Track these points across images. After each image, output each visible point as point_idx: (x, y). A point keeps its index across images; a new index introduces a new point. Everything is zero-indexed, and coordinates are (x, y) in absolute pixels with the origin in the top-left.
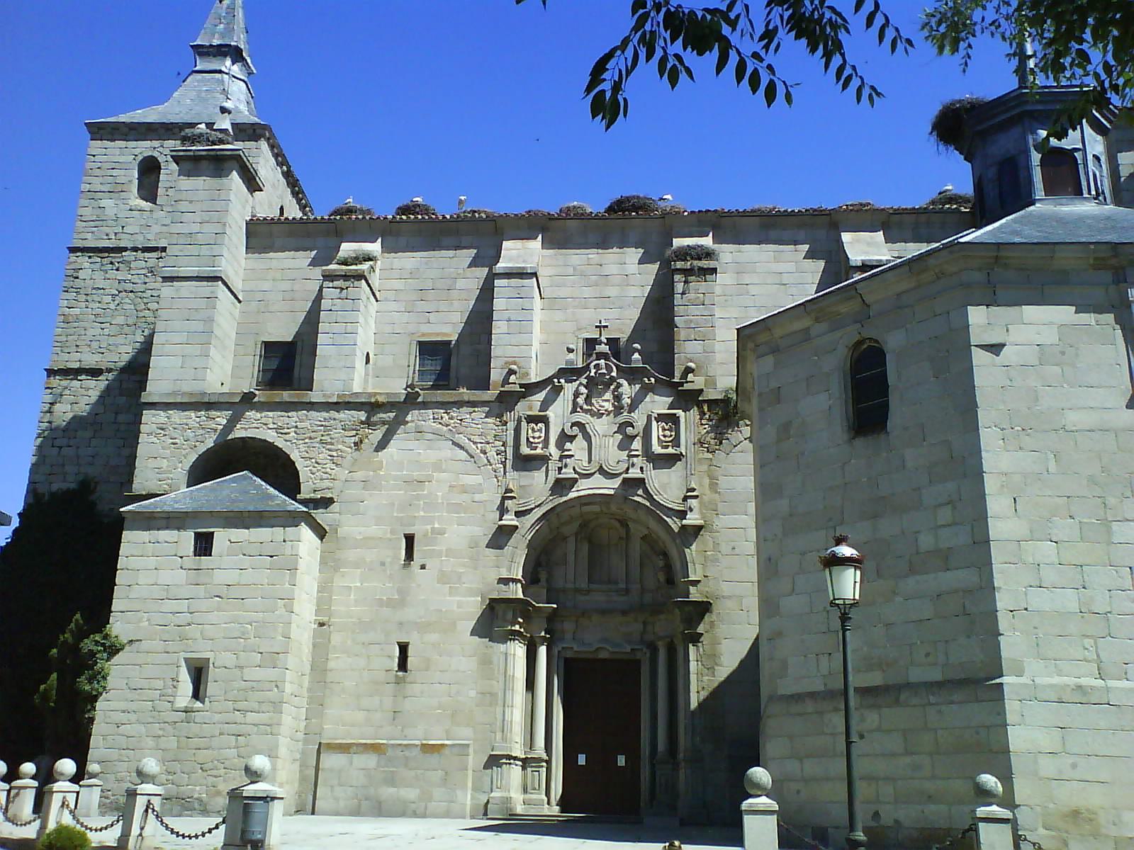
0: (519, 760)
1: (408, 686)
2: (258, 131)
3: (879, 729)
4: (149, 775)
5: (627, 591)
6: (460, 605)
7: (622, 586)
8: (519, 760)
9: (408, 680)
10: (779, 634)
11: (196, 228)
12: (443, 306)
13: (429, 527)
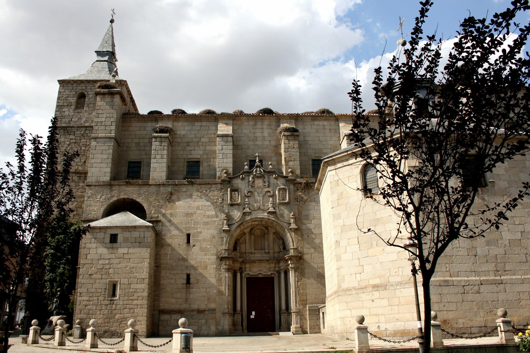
0: (227, 313)
1: (191, 290)
2: (122, 83)
3: (379, 298)
4: (152, 321)
5: (269, 253)
6: (209, 259)
7: (267, 251)
8: (227, 313)
9: (191, 287)
10: (341, 267)
11: (104, 120)
12: (196, 148)
13: (196, 231)
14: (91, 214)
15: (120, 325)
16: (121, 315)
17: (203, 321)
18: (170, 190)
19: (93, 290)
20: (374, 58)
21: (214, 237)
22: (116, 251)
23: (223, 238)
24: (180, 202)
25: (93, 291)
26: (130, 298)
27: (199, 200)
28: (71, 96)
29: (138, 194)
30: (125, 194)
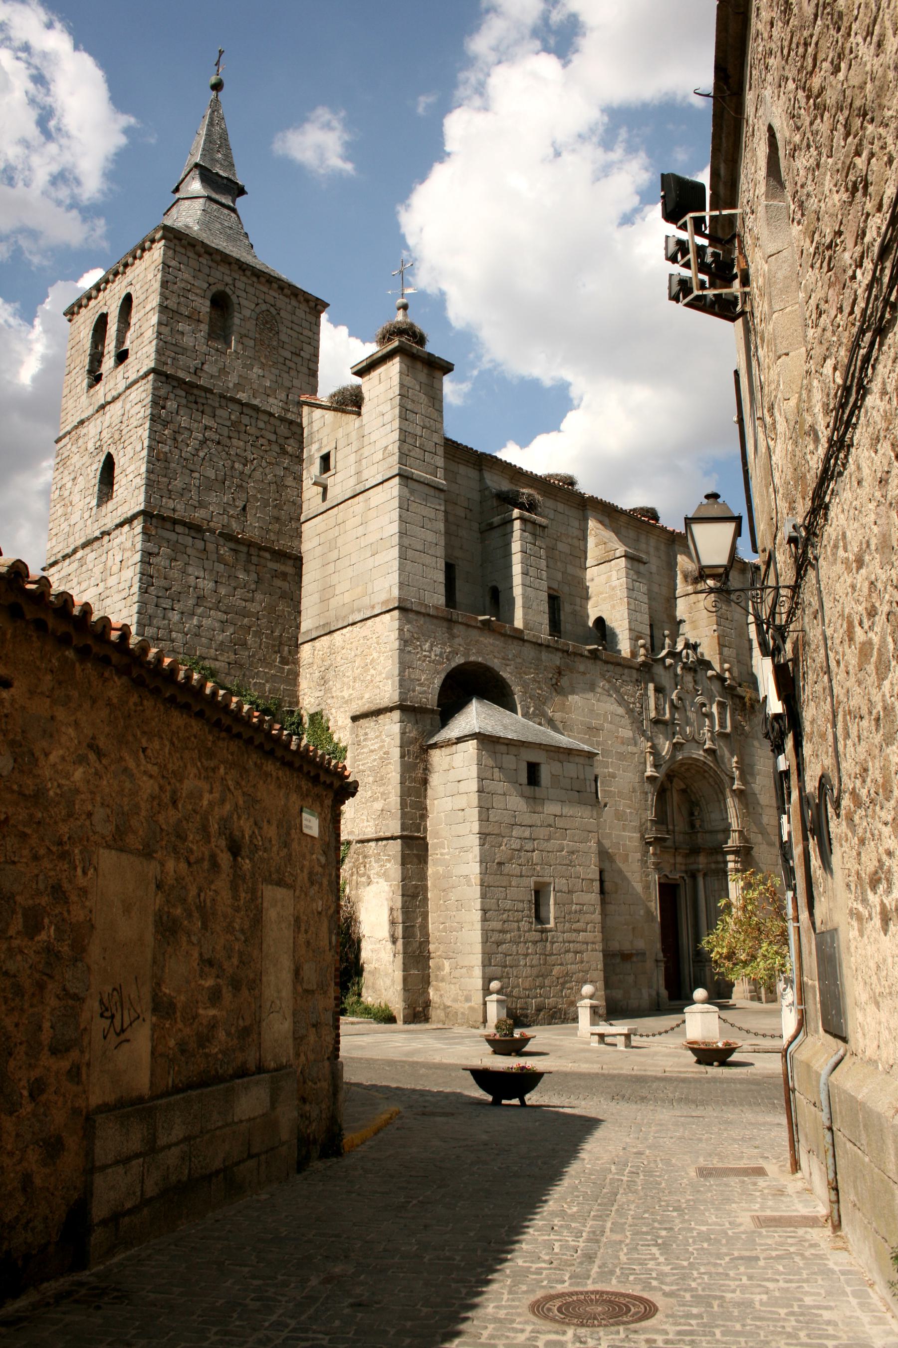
14: (414, 691)
15: (562, 991)
16: (563, 968)
17: (630, 979)
18: (558, 663)
19: (508, 904)
20: (351, 335)
21: (634, 791)
22: (540, 809)
23: (646, 793)
24: (576, 697)
25: (508, 908)
26: (574, 926)
27: (605, 698)
28: (198, 291)
29: (503, 659)
30: (479, 653)
